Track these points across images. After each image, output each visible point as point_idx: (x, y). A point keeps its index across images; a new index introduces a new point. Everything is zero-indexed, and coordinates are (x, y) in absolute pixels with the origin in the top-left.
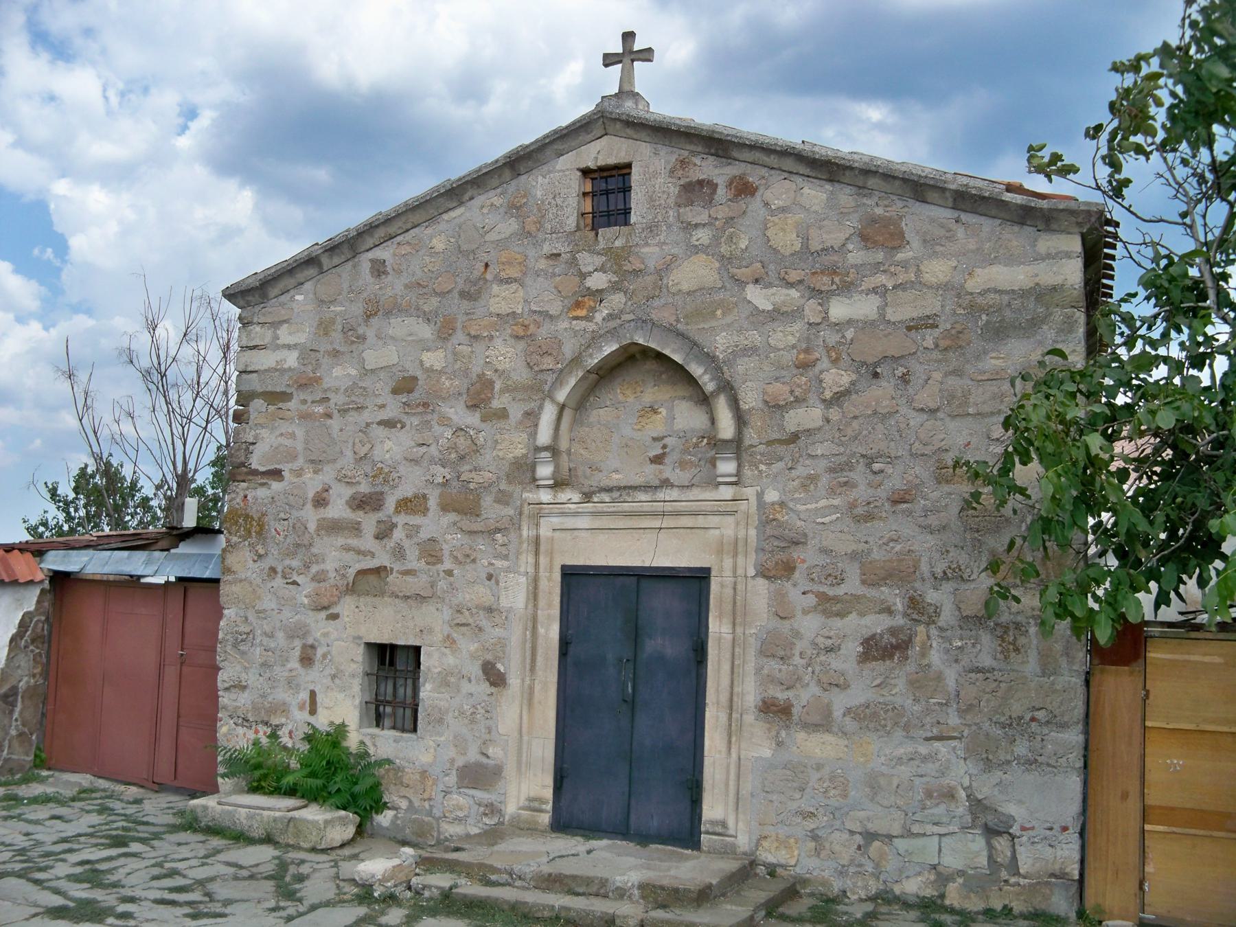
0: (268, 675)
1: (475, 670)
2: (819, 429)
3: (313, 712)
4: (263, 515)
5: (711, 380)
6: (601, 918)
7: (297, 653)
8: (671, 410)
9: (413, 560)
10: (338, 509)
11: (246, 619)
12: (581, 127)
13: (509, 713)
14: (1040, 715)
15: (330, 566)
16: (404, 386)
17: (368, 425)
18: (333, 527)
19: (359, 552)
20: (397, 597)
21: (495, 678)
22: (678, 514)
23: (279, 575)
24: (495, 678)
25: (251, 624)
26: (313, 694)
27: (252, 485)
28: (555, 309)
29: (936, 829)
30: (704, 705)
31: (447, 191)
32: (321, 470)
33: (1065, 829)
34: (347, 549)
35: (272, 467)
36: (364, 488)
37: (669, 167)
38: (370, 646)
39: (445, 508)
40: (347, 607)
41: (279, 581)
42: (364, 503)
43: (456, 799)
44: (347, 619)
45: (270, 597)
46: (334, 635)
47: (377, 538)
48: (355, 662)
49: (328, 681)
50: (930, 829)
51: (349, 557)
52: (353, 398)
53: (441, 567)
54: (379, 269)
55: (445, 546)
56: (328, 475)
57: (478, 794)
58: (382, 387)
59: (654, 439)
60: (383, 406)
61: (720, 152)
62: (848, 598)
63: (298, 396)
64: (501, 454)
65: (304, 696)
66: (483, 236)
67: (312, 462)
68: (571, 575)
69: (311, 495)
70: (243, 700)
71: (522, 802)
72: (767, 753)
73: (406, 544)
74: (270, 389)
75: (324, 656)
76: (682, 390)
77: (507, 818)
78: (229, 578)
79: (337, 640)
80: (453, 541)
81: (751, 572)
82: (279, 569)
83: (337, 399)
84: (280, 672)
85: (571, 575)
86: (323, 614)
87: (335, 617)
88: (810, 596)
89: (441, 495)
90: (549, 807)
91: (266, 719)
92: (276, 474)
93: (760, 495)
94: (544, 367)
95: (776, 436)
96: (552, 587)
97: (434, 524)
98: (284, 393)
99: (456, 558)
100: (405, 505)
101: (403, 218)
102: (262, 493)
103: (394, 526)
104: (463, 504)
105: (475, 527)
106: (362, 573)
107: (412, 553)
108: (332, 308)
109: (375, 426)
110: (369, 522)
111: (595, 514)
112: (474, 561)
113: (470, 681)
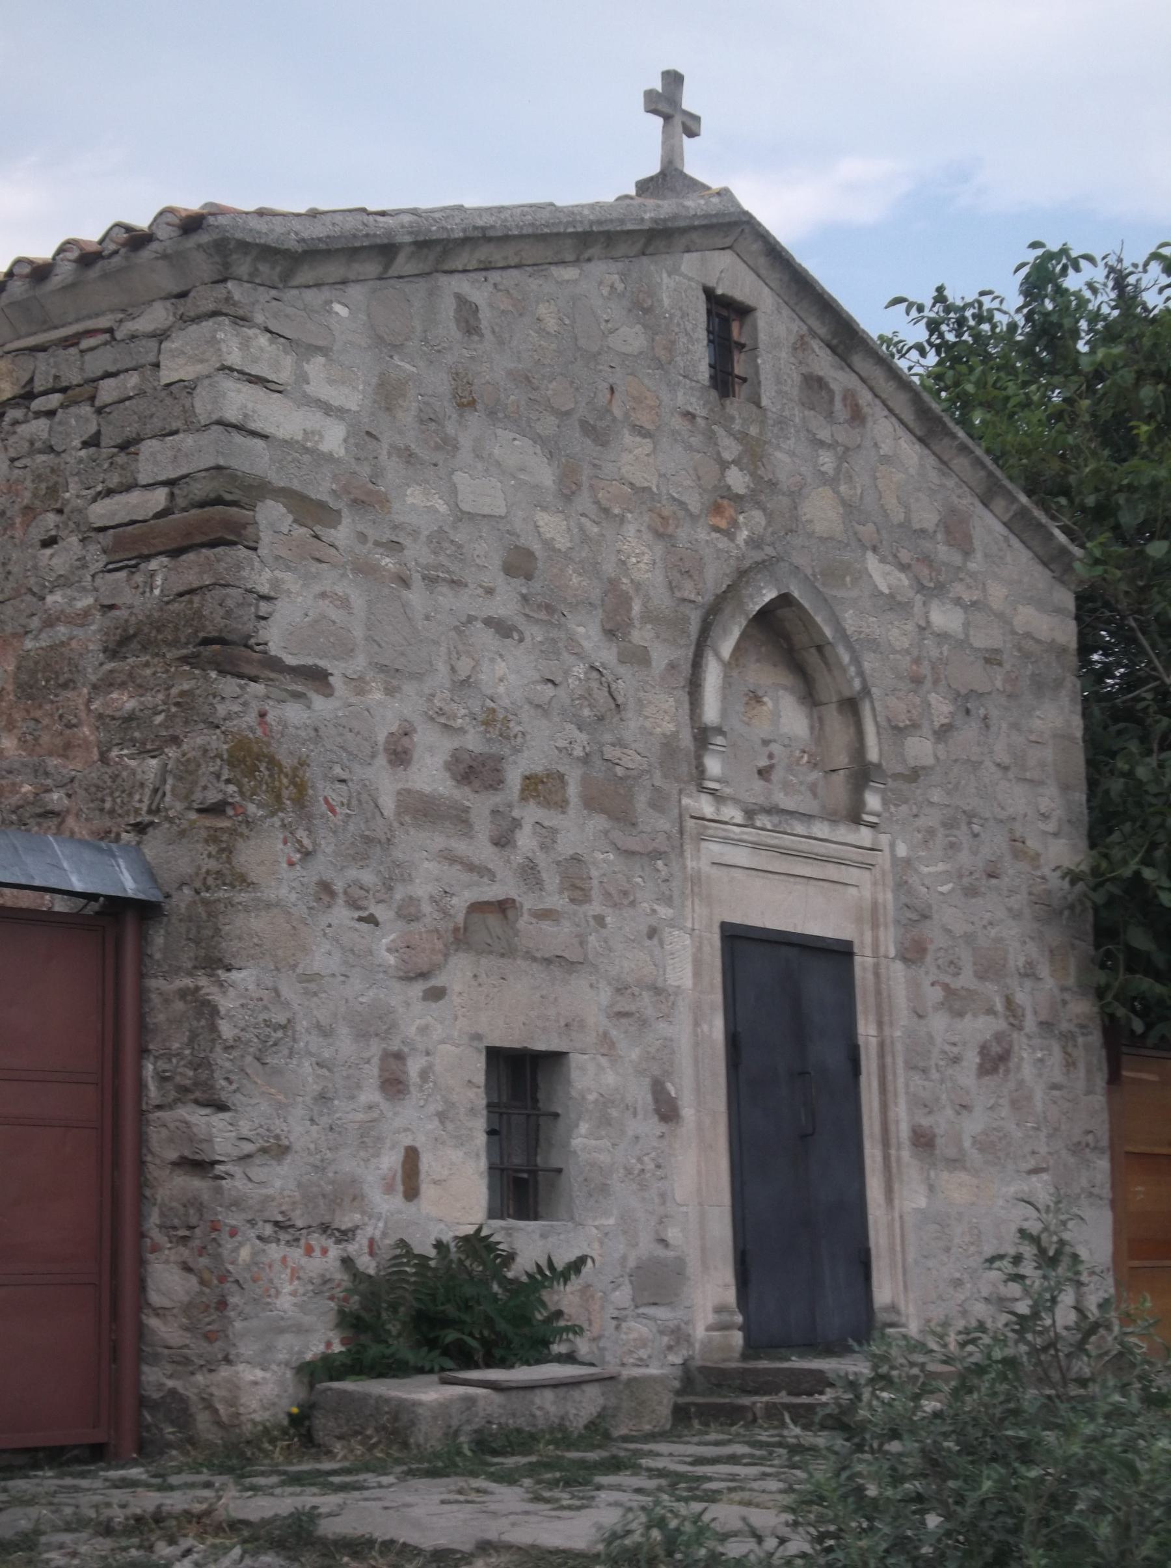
0: (325, 1121)
3: (412, 1193)
4: (303, 763)
7: (372, 1072)
8: (776, 702)
10: (430, 774)
11: (278, 994)
15: (422, 889)
16: (519, 564)
17: (471, 619)
19: (471, 867)
20: (534, 959)
21: (667, 1111)
22: (825, 860)
23: (341, 901)
25: (287, 1005)
26: (412, 1156)
27: (275, 693)
28: (694, 503)
32: (398, 689)
34: (450, 858)
35: (310, 661)
38: (495, 1055)
39: (591, 803)
40: (458, 974)
41: (341, 914)
43: (637, 1329)
44: (457, 1000)
45: (326, 946)
46: (438, 1032)
47: (496, 844)
48: (466, 1082)
52: (442, 559)
55: (594, 873)
57: (661, 1313)
58: (487, 554)
60: (490, 592)
61: (840, 349)
62: (964, 993)
64: (648, 724)
65: (390, 1161)
66: (605, 336)
67: (383, 668)
69: (381, 737)
70: (279, 1182)
71: (711, 1318)
72: (922, 1202)
73: (542, 860)
74: (296, 485)
75: (424, 1074)
77: (697, 1346)
78: (243, 897)
79: (442, 1042)
80: (603, 863)
81: (892, 952)
82: (339, 886)
83: (417, 553)
84: (349, 1113)
85: (736, 939)
86: (419, 988)
87: (436, 994)
88: (938, 988)
91: (327, 1219)
92: (317, 677)
97: (578, 831)
98: (322, 505)
99: (608, 894)
100: (539, 787)
102: (293, 713)
103: (517, 824)
104: (611, 799)
105: (632, 844)
106: (477, 908)
107: (551, 880)
109: (479, 625)
110: (480, 805)
111: (756, 846)
112: (633, 904)
113: (635, 1114)
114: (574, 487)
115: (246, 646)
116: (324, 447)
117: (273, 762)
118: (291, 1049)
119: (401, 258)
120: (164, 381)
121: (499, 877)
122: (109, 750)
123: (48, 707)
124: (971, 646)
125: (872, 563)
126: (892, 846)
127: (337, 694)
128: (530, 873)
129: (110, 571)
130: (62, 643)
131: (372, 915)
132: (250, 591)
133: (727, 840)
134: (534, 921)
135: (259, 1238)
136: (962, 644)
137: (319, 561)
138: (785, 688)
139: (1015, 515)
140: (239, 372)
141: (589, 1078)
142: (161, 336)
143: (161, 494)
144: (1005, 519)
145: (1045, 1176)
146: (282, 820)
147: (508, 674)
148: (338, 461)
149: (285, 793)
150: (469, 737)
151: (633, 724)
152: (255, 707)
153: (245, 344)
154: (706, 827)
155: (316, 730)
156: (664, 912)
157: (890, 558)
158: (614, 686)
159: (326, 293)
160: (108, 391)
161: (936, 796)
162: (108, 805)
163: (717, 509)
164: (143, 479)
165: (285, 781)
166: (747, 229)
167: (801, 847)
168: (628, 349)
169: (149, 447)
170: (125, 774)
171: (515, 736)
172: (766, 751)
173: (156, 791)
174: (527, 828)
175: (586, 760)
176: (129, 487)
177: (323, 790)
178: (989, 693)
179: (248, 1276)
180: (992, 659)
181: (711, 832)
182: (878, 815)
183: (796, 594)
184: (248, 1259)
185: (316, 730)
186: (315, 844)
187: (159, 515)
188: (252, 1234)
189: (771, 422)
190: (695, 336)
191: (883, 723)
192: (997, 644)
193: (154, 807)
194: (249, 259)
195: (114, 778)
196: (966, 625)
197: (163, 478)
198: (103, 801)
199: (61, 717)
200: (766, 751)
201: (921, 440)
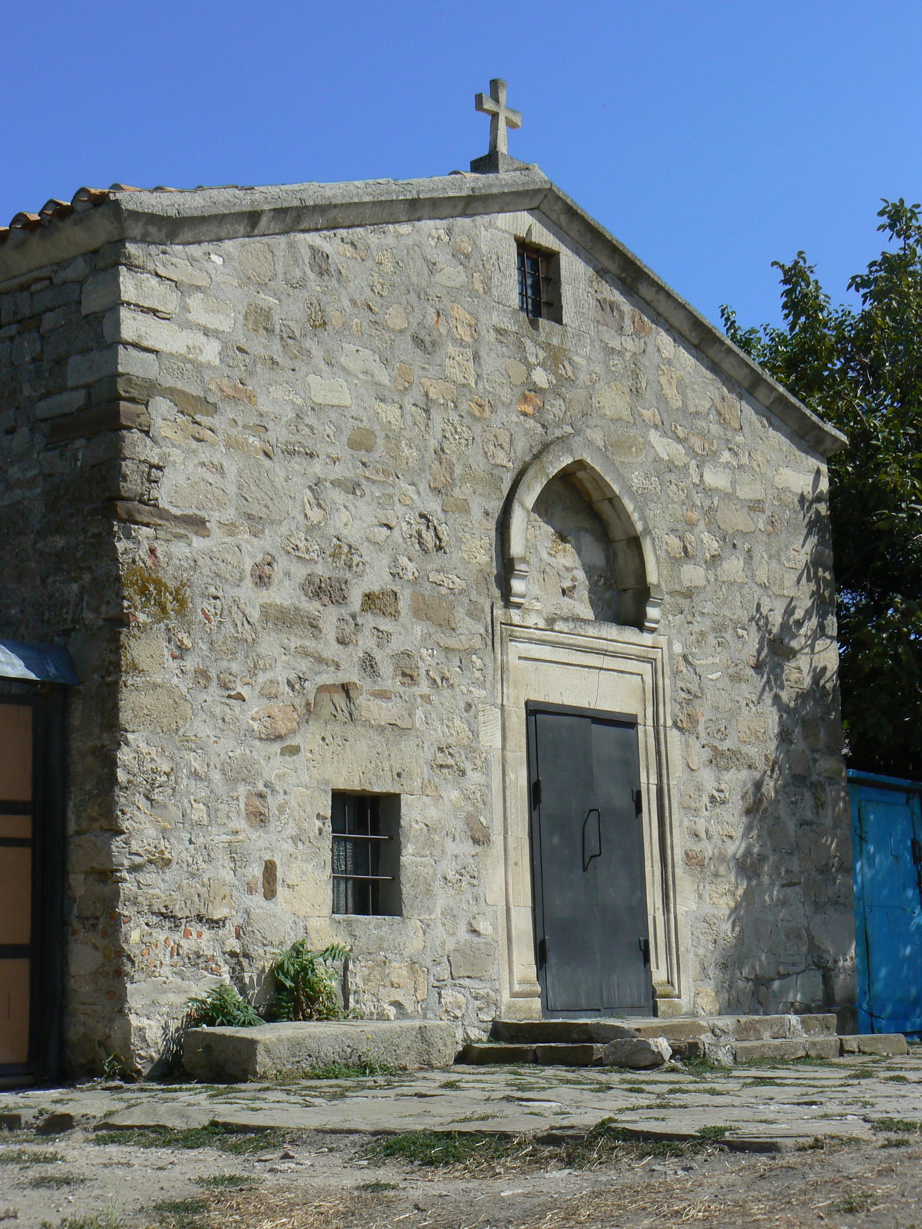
1: (459, 826)
3: (270, 894)
6: (116, 683)
9: (389, 679)
16: (361, 442)
18: (281, 619)
21: (480, 838)
22: (614, 655)
23: (214, 683)
24: (480, 838)
26: (270, 869)
36: (321, 570)
38: (340, 798)
40: (308, 739)
42: (326, 591)
49: (288, 846)
51: (304, 665)
53: (416, 690)
56: (269, 541)
63: (229, 412)
65: (256, 871)
68: (534, 710)
69: (248, 566)
72: (694, 906)
73: (378, 655)
75: (281, 809)
77: (503, 1009)
82: (213, 674)
85: (534, 710)
86: (276, 747)
87: (294, 751)
89: (413, 594)
92: (198, 524)
95: (677, 588)
97: (408, 633)
102: (179, 550)
107: (386, 668)
108: (262, 295)
110: (330, 619)
114: (407, 385)
115: (141, 502)
116: (202, 359)
117: (158, 583)
118: (174, 789)
119: (264, 221)
120: (83, 314)
121: (342, 668)
122: (47, 577)
123: (9, 548)
124: (738, 498)
125: (654, 437)
126: (670, 644)
127: (212, 536)
128: (369, 665)
129: (49, 450)
130: (19, 503)
131: (239, 693)
132: (145, 462)
133: (531, 641)
134: (372, 698)
135: (147, 924)
136: (728, 496)
137: (199, 440)
138: (586, 530)
139: (774, 401)
140: (136, 305)
141: (414, 814)
142: (81, 282)
143: (82, 393)
144: (768, 404)
145: (797, 889)
146: (167, 625)
147: (353, 520)
148: (215, 368)
149: (169, 607)
150: (319, 566)
151: (455, 556)
152: (145, 545)
153: (139, 286)
154: (512, 631)
155: (195, 561)
156: (478, 692)
157: (670, 434)
158: (439, 528)
159: (205, 246)
160: (49, 321)
161: (708, 608)
162: (46, 617)
163: (525, 399)
164: (70, 384)
165: (170, 598)
166: (550, 195)
167: (594, 646)
168: (451, 284)
169: (74, 361)
170: (57, 595)
171: (357, 565)
172: (569, 576)
173: (77, 606)
174: (367, 632)
175: (415, 582)
176: (63, 389)
177: (199, 605)
178: (754, 532)
179: (138, 952)
180: (755, 506)
181: (518, 634)
182: (657, 622)
183: (589, 461)
184: (138, 940)
185: (195, 561)
186: (194, 642)
187: (79, 410)
188: (142, 921)
189: (570, 335)
190: (508, 273)
191: (662, 554)
192: (759, 496)
193: (75, 618)
194: (140, 224)
195: (50, 597)
196: (733, 483)
197: (82, 382)
198: (43, 614)
199: (17, 555)
200: (569, 576)
201: (696, 347)
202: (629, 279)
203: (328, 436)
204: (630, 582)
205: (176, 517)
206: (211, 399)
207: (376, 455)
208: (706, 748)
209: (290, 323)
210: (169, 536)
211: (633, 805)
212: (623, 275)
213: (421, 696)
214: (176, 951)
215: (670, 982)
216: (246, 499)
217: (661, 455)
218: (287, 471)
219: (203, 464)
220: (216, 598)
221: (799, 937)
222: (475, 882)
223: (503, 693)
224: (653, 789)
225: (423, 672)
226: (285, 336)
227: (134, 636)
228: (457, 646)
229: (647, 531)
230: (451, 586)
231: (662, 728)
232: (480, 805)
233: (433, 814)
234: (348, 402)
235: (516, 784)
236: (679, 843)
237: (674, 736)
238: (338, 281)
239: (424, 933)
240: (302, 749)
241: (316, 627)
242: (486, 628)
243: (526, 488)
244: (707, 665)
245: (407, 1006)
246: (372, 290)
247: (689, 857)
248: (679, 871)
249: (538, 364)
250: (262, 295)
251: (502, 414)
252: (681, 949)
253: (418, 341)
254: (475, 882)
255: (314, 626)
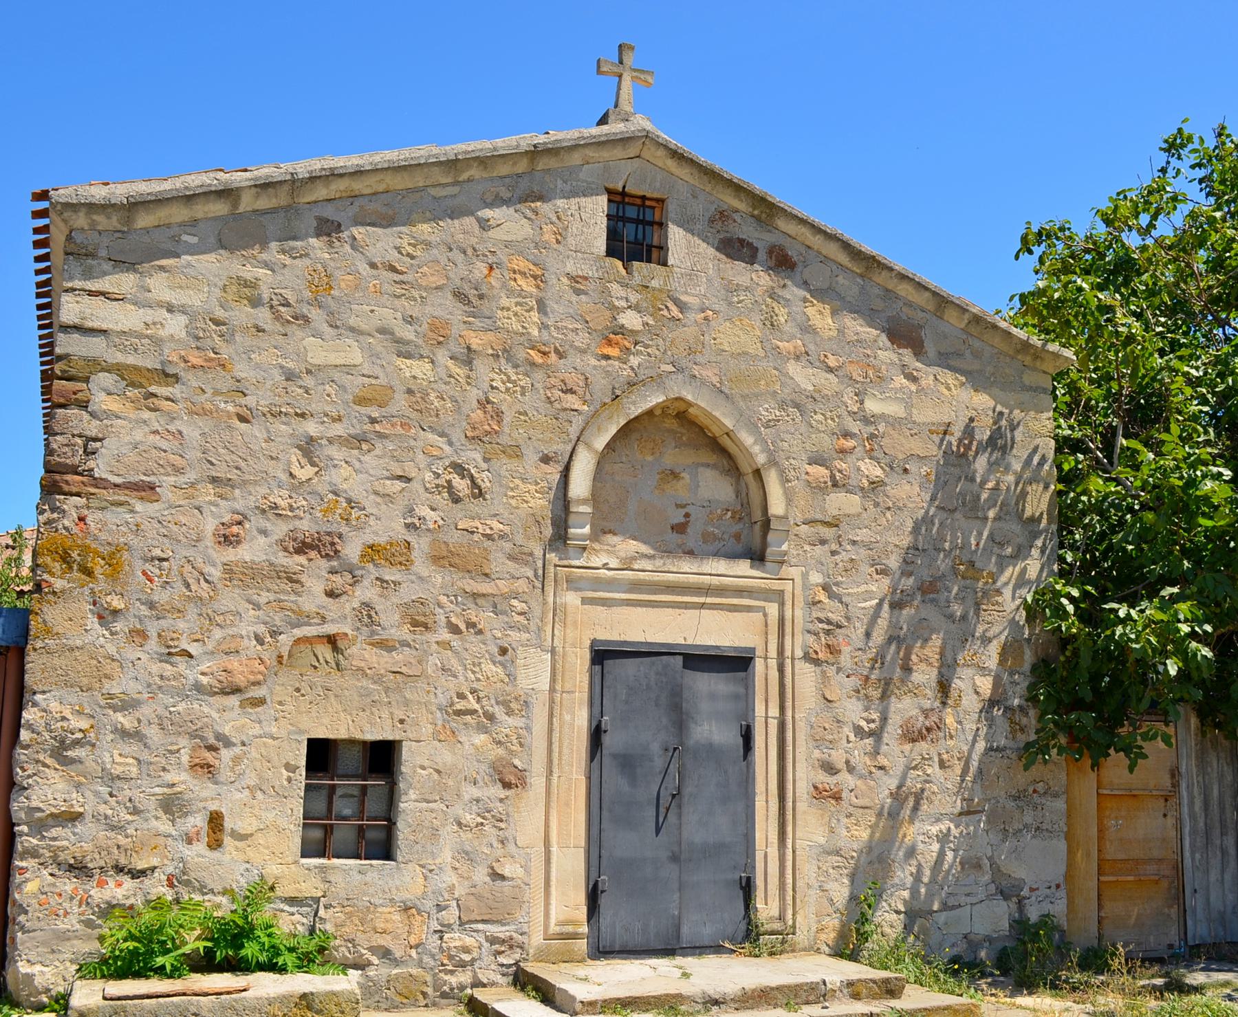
2: (859, 515)
5: (762, 451)
12: (622, 140)
13: (528, 818)
14: (1040, 787)
29: (969, 900)
30: (754, 794)
31: (449, 161)
33: (1058, 886)
36: (306, 526)
37: (708, 215)
40: (279, 689)
50: (963, 900)
53: (432, 637)
54: (484, 225)
56: (241, 501)
59: (678, 506)
65: (198, 821)
67: (214, 480)
76: (712, 458)
77: (531, 951)
86: (234, 700)
90: (585, 929)
92: (146, 490)
93: (805, 576)
94: (568, 406)
95: (819, 516)
96: (580, 661)
97: (426, 581)
101: (380, 176)
102: (114, 517)
134: (368, 647)
147: (351, 475)
202: (764, 216)
203: (328, 395)
204: (757, 515)
205: (116, 486)
206: (171, 370)
207: (392, 409)
208: (853, 678)
209: (283, 291)
210: (104, 504)
211: (740, 741)
212: (756, 212)
213: (437, 643)
214: (86, 902)
215: (781, 918)
216: (212, 464)
217: (803, 386)
218: (268, 432)
219: (156, 432)
220: (161, 560)
221: (978, 866)
222: (502, 825)
223: (553, 635)
224: (773, 724)
225: (442, 619)
226: (275, 303)
227: (48, 602)
228: (490, 591)
229: (773, 462)
230: (488, 532)
231: (788, 661)
232: (516, 748)
233: (446, 757)
234: (358, 360)
235: (572, 725)
236: (803, 776)
237: (805, 669)
238: (353, 247)
239: (426, 878)
240: (268, 700)
241: (297, 582)
242: (535, 570)
243: (595, 430)
244: (858, 594)
245: (395, 951)
246: (400, 253)
247: (819, 793)
248: (801, 806)
249: (630, 307)
250: (249, 267)
251: (574, 359)
252: (799, 884)
253: (459, 295)
254: (502, 825)
255: (292, 579)
